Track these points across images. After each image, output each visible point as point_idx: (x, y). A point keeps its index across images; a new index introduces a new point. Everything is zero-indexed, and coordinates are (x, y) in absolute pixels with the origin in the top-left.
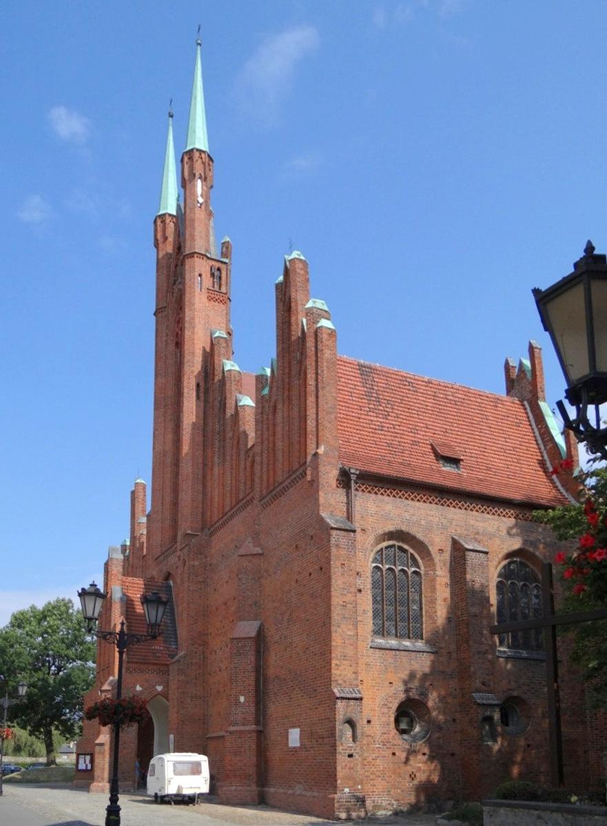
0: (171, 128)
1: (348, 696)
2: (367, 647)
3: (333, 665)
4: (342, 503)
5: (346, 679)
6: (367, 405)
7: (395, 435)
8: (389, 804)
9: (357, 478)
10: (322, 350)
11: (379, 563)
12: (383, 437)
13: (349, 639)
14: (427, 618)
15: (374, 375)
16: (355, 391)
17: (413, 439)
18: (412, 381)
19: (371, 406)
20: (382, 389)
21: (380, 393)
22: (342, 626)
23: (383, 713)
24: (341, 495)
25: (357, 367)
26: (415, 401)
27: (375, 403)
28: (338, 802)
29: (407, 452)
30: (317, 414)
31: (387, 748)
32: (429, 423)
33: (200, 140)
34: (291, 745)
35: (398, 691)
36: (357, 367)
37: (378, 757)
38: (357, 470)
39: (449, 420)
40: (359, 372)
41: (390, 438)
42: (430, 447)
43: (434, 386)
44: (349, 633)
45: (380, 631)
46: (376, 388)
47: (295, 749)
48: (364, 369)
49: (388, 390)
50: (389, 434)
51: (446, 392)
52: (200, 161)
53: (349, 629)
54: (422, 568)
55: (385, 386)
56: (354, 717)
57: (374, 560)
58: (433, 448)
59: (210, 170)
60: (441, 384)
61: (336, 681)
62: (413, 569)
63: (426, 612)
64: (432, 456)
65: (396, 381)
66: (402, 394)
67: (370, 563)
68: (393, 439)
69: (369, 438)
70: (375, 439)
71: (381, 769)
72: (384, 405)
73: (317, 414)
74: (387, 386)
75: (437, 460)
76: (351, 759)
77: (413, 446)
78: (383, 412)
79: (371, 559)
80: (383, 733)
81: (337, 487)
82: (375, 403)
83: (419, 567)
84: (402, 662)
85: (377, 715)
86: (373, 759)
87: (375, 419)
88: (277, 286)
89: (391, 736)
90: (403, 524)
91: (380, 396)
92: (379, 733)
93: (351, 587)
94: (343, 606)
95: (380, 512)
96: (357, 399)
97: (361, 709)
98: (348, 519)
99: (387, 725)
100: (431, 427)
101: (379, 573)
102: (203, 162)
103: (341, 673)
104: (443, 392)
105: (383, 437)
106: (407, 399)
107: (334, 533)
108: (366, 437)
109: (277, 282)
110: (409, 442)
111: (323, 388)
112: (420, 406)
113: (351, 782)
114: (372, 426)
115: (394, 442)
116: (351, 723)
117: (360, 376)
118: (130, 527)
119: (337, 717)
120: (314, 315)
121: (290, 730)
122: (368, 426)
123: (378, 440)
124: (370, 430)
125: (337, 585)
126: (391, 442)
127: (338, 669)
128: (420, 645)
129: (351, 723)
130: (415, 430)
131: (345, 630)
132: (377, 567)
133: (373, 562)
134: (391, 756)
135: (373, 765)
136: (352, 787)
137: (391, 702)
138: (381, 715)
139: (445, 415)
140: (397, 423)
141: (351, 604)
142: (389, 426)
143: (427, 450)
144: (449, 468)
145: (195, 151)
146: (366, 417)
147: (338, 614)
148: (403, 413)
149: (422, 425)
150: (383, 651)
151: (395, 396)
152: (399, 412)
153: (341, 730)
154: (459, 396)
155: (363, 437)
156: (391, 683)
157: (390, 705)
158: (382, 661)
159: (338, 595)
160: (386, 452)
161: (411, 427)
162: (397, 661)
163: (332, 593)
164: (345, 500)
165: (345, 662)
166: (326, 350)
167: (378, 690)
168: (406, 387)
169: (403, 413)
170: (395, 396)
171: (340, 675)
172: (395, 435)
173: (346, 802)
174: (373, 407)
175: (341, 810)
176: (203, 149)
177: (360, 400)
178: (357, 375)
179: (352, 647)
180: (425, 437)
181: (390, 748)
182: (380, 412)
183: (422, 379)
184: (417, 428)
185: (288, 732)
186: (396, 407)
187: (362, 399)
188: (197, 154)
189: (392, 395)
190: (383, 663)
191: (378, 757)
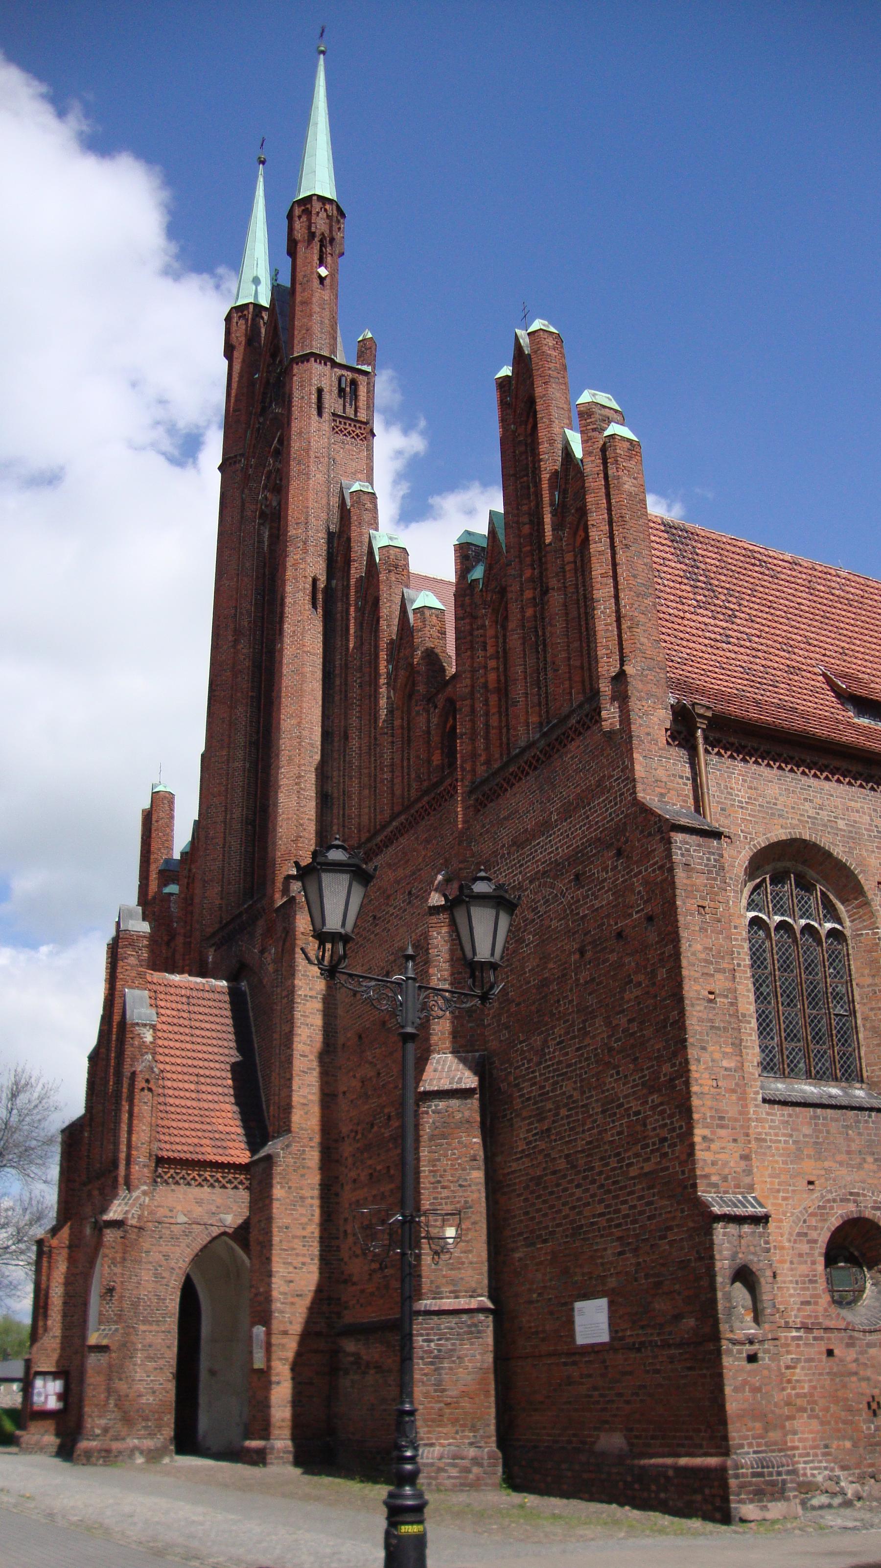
0: (261, 180)
1: (739, 1211)
2: (756, 1099)
3: (697, 1139)
4: (681, 777)
5: (726, 1171)
6: (691, 596)
7: (754, 653)
8: (830, 1479)
9: (709, 726)
10: (618, 478)
11: (760, 911)
12: (733, 656)
13: (725, 1077)
14: (870, 1034)
15: (695, 544)
16: (665, 569)
17: (789, 662)
18: (765, 558)
19: (699, 598)
20: (715, 569)
21: (712, 575)
22: (711, 1048)
23: (800, 1255)
24: (675, 762)
25: (663, 528)
26: (778, 594)
27: (707, 593)
28: (737, 1476)
29: (782, 686)
30: (617, 597)
31: (815, 1339)
32: (812, 635)
33: (319, 178)
34: (581, 1339)
35: (828, 1201)
36: (663, 528)
37: (798, 1360)
38: (708, 708)
39: (845, 632)
40: (666, 535)
41: (746, 658)
42: (821, 678)
43: (805, 571)
44: (725, 1063)
45: (768, 1066)
46: (703, 566)
47: (594, 1349)
48: (675, 531)
49: (726, 572)
50: (742, 650)
51: (829, 583)
52: (323, 215)
53: (725, 1054)
54: (848, 923)
55: (718, 563)
56: (757, 1264)
57: (749, 904)
58: (829, 681)
59: (339, 229)
60: (817, 567)
61: (707, 1176)
62: (829, 926)
63: (865, 1019)
64: (831, 696)
65: (737, 557)
66: (752, 580)
67: (743, 911)
68: (752, 659)
69: (707, 656)
70: (719, 659)
71: (806, 1391)
72: (724, 598)
73: (617, 597)
74: (723, 565)
75: (842, 704)
76: (753, 1366)
77: (791, 676)
78: (724, 611)
79: (744, 902)
80: (802, 1303)
81: (668, 743)
82: (707, 593)
83: (839, 921)
84: (828, 1132)
85: (788, 1258)
86: (788, 1367)
87: (712, 621)
88: (503, 384)
89: (820, 1309)
90: (804, 827)
91: (712, 581)
92: (794, 1301)
93: (723, 958)
94: (711, 1001)
95: (757, 802)
96: (672, 584)
97: (767, 1242)
98: (697, 810)
99: (811, 1281)
100: (816, 643)
101: (761, 933)
102: (328, 216)
103: (715, 1155)
104: (823, 582)
105: (733, 656)
106: (762, 589)
107: (678, 838)
108: (701, 654)
109: (498, 376)
110: (781, 667)
111: (627, 546)
112: (787, 603)
113: (758, 1425)
114: (708, 634)
115: (755, 667)
116: (745, 1276)
117: (670, 544)
118: (100, 1011)
119: (718, 1265)
120: (589, 419)
121: (578, 1305)
122: (700, 633)
123: (725, 660)
124: (707, 642)
125: (694, 954)
126: (750, 666)
127: (708, 1149)
128: (859, 1094)
129: (745, 1276)
130: (788, 647)
131: (717, 1056)
132: (755, 921)
133: (748, 910)
134: (824, 1357)
135: (789, 1381)
136: (762, 1437)
137: (816, 1228)
138: (795, 1260)
139: (837, 624)
140: (754, 632)
141: (726, 997)
142: (739, 635)
143: (818, 684)
144: (867, 721)
145: (315, 198)
146: (694, 617)
147: (700, 1020)
148: (760, 614)
149: (799, 638)
150: (790, 1110)
151: (741, 583)
152: (755, 613)
153: (728, 1297)
154: (853, 590)
155: (695, 653)
156: (811, 1183)
157: (814, 1235)
158: (789, 1131)
159: (697, 975)
160: (746, 682)
161: (781, 640)
162: (821, 1132)
163: (685, 972)
164: (688, 772)
165: (722, 1132)
166: (625, 478)
167: (785, 1199)
168: (757, 569)
169: (760, 614)
170: (741, 583)
171: (714, 1163)
172: (754, 653)
173: (754, 1475)
174: (704, 599)
175: (743, 1496)
176: (328, 195)
177: (678, 586)
178: (664, 542)
179: (734, 1097)
180: (809, 661)
181: (821, 1339)
182: (719, 610)
183: (781, 557)
184: (792, 643)
185: (572, 1310)
186: (746, 603)
187: (680, 583)
188: (317, 206)
189: (735, 581)
190: (791, 1136)
191: (798, 1360)
